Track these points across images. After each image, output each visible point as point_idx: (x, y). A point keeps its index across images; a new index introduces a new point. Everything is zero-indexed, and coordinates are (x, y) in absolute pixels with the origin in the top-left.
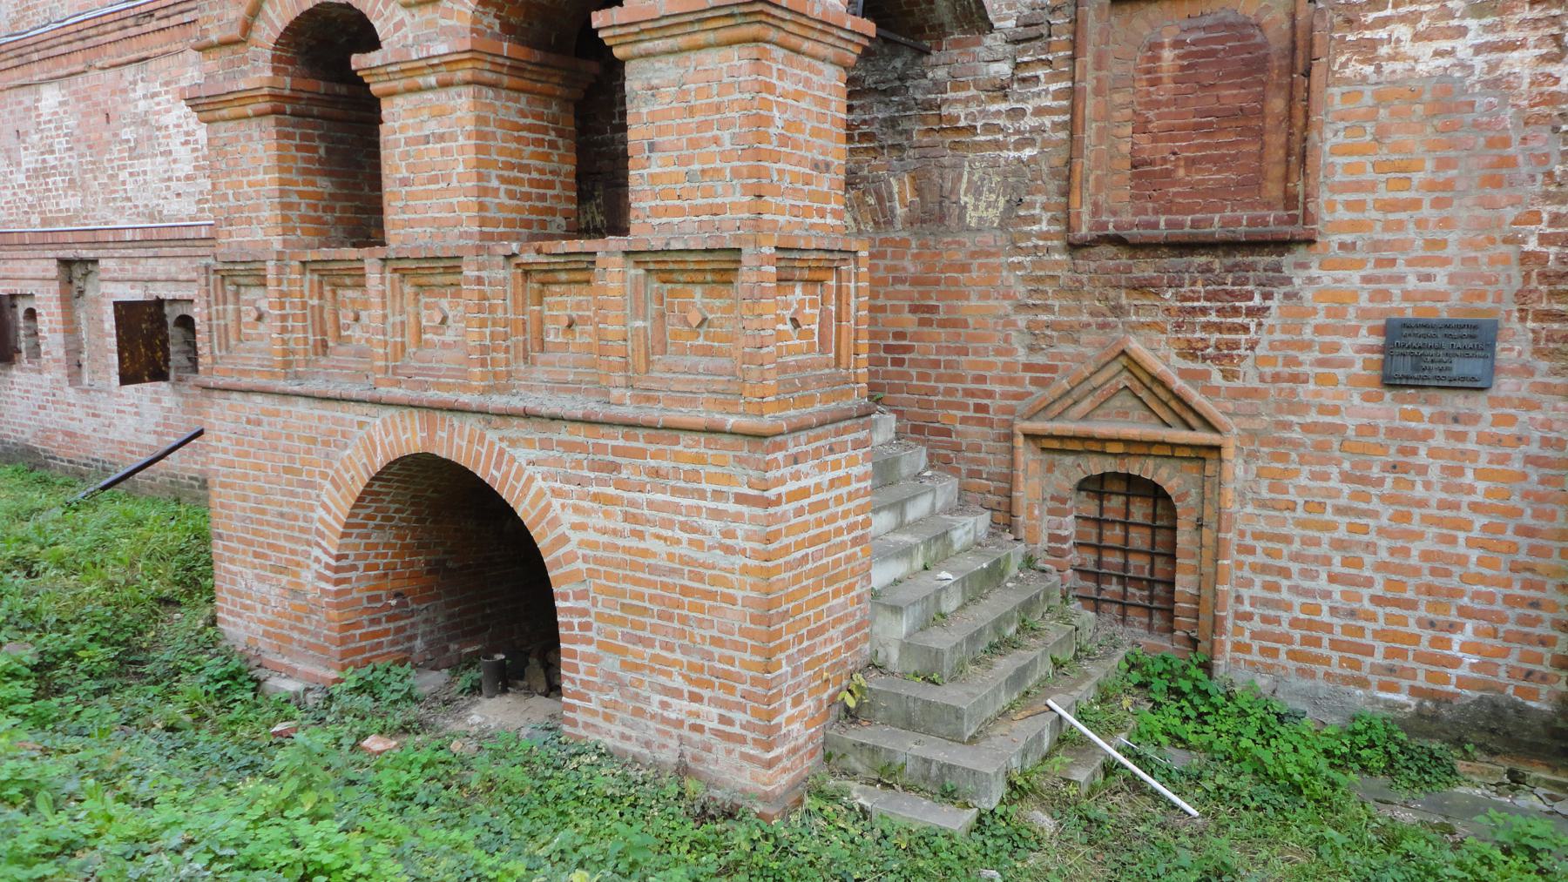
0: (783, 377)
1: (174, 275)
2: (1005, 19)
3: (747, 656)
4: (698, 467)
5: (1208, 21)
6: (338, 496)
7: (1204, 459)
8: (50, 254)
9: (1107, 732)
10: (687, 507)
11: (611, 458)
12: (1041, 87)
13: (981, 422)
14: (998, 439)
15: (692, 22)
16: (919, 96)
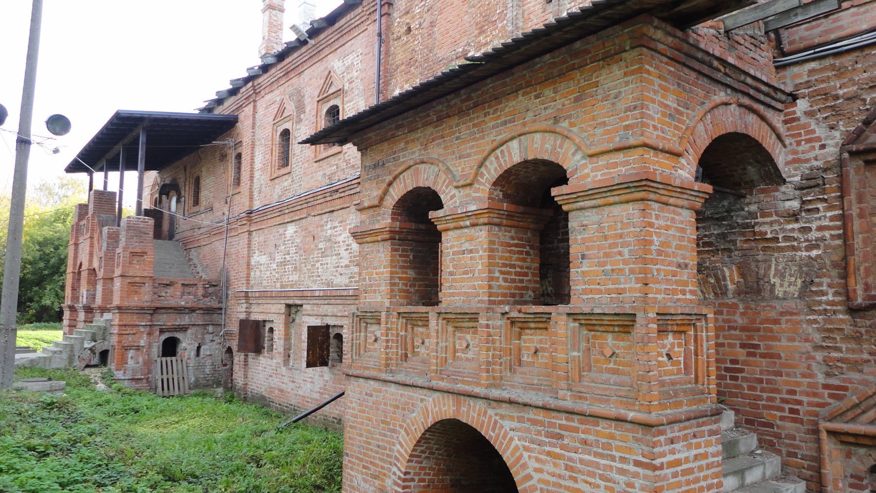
0: (662, 389)
1: (335, 314)
4: (611, 441)
8: (283, 302)
10: (604, 465)
11: (558, 431)
12: (820, 214)
13: (794, 420)
14: (808, 432)
15: (606, 192)
16: (740, 221)
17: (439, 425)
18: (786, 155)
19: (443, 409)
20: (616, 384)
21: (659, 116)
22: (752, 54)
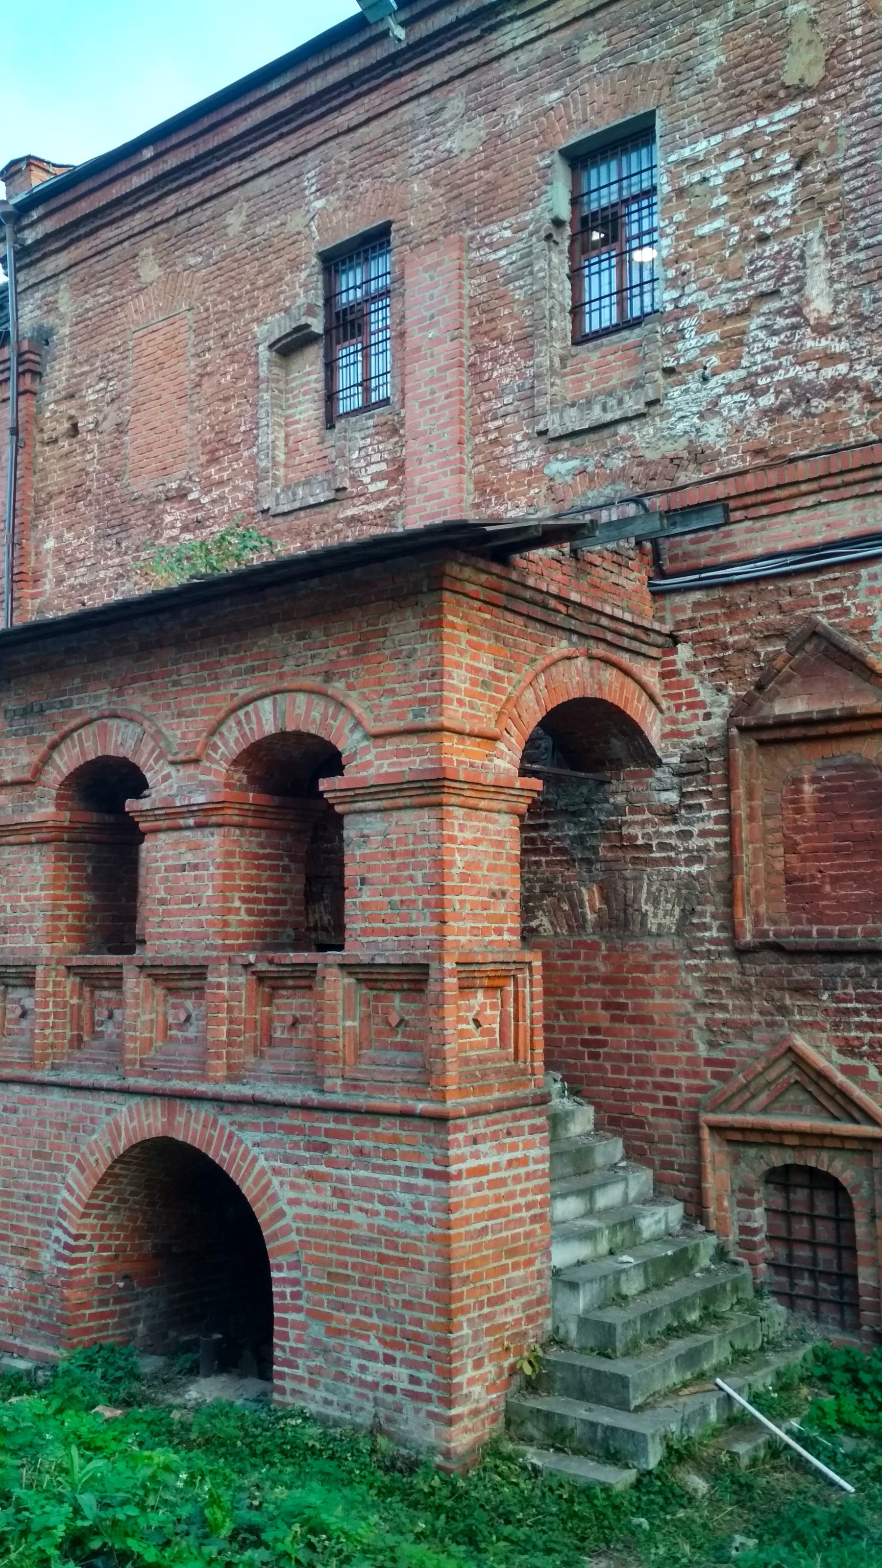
0: (466, 1069)
2: (671, 756)
3: (432, 1318)
4: (394, 1146)
5: (838, 762)
6: (81, 1178)
7: (870, 1151)
9: (777, 1417)
11: (323, 1139)
13: (671, 1114)
16: (602, 818)
17: (137, 1150)
18: (663, 724)
19: (146, 1123)
20: (404, 1065)
21: (467, 685)
22: (613, 578)
